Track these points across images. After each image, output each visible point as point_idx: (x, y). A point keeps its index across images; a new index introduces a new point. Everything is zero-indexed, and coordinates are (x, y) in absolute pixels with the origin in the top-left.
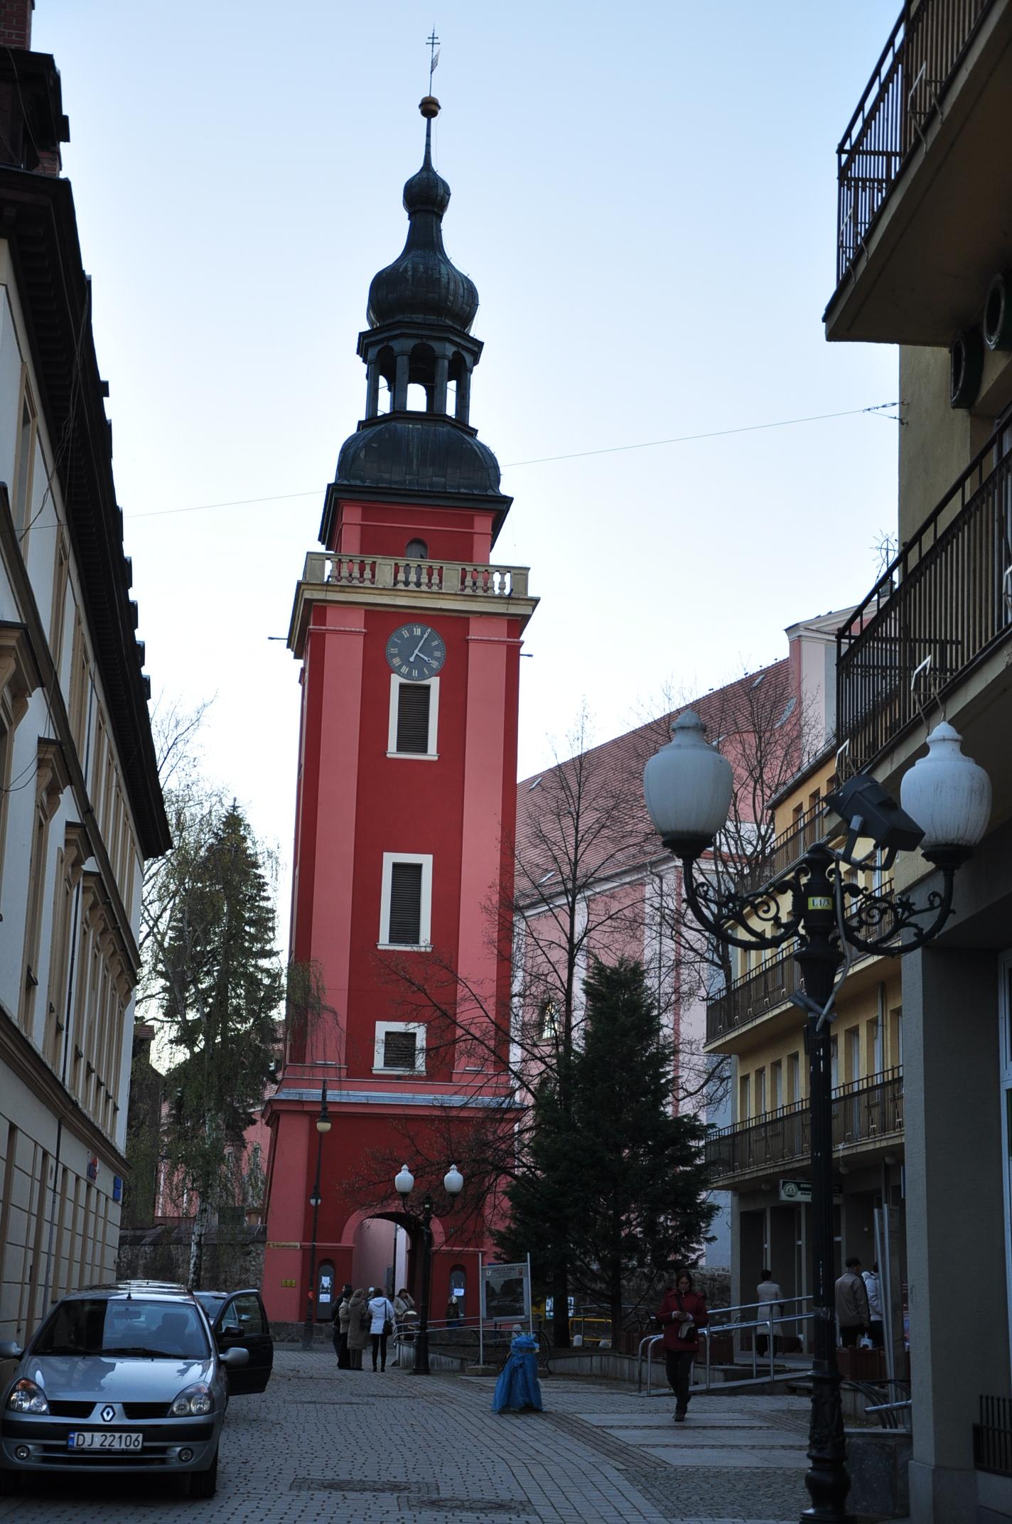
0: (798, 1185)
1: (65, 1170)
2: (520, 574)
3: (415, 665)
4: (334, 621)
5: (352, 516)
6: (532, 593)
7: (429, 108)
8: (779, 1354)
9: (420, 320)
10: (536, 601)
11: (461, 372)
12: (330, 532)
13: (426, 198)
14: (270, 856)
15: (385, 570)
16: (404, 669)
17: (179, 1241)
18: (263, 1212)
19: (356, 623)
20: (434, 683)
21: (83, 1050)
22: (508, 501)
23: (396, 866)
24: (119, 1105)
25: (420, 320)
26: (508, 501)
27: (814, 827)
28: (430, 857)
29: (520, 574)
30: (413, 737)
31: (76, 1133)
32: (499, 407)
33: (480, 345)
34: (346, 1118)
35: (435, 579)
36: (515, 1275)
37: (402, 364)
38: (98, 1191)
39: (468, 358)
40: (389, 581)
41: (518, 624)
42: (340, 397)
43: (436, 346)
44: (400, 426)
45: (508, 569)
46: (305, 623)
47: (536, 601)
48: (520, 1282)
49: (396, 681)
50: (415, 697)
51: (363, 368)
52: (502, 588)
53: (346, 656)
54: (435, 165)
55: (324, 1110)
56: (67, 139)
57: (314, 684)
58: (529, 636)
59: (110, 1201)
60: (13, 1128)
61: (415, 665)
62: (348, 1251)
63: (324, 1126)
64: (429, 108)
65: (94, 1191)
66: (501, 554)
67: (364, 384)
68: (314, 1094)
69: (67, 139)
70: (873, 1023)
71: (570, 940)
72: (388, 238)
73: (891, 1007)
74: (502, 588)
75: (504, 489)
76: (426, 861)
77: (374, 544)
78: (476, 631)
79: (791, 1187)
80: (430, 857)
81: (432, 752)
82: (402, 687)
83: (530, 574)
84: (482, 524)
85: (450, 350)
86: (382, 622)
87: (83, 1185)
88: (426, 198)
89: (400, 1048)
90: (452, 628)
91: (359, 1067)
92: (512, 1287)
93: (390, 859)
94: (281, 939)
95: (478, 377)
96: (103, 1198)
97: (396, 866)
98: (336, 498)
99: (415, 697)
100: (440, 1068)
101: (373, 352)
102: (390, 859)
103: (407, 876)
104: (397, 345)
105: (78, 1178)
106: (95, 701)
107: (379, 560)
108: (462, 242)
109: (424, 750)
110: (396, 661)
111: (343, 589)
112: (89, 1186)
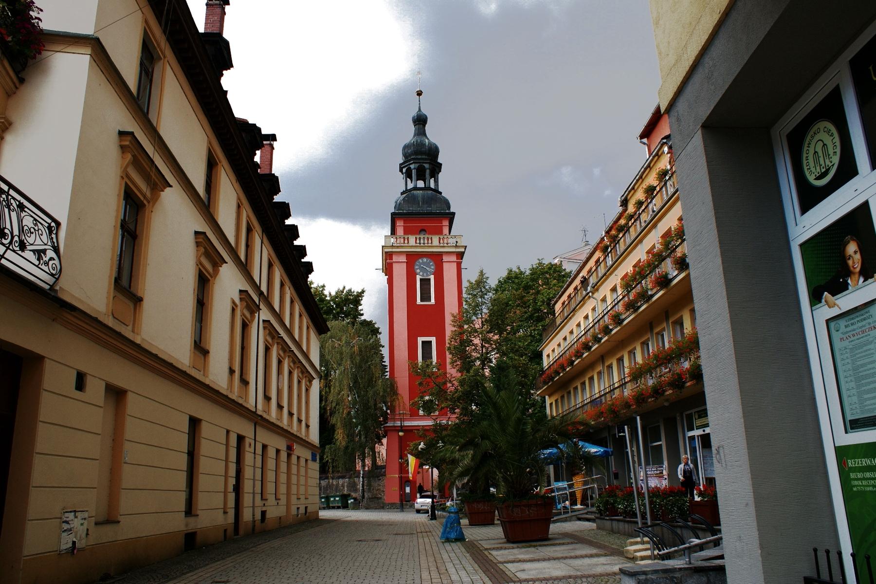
1: (265, 447)
3: (424, 270)
4: (395, 258)
5: (400, 223)
7: (419, 94)
8: (670, 277)
13: (420, 121)
14: (483, 438)
15: (412, 240)
20: (432, 277)
22: (454, 214)
23: (423, 342)
24: (311, 424)
26: (454, 214)
30: (425, 296)
31: (263, 426)
32: (448, 184)
37: (414, 172)
38: (298, 458)
39: (437, 170)
41: (461, 255)
44: (415, 192)
46: (386, 260)
49: (418, 278)
50: (425, 282)
53: (400, 271)
55: (402, 428)
56: (228, 4)
57: (390, 282)
59: (310, 462)
60: (228, 432)
61: (424, 270)
63: (401, 434)
64: (419, 94)
65: (294, 459)
67: (404, 182)
69: (228, 4)
70: (599, 373)
72: (408, 134)
73: (607, 364)
75: (452, 210)
76: (433, 339)
77: (408, 231)
78: (445, 258)
81: (433, 301)
82: (421, 280)
86: (412, 258)
87: (284, 455)
88: (420, 121)
90: (437, 258)
93: (420, 340)
97: (423, 342)
99: (425, 282)
101: (404, 170)
102: (420, 340)
103: (427, 345)
104: (412, 166)
105: (278, 451)
107: (410, 237)
108: (433, 134)
109: (430, 300)
110: (418, 271)
111: (398, 247)
112: (289, 456)
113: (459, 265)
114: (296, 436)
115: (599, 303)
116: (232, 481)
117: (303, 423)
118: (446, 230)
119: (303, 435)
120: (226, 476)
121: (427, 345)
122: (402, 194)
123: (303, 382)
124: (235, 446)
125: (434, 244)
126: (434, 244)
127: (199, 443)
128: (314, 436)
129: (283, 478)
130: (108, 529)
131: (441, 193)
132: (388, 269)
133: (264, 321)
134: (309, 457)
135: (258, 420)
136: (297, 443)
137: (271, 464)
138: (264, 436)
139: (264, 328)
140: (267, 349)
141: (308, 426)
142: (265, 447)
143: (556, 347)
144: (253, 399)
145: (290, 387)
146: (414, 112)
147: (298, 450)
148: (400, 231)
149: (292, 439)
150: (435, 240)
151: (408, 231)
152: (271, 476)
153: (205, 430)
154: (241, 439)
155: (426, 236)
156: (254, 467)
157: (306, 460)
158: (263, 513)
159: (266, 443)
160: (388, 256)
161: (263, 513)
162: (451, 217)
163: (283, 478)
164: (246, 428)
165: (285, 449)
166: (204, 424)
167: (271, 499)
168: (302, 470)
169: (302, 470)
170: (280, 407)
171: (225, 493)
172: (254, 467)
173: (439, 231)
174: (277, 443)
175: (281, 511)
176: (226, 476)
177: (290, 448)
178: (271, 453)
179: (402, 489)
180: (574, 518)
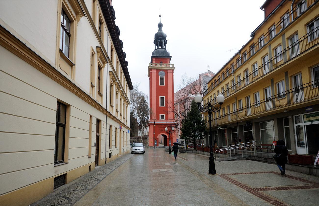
0: (220, 127)
2: (173, 64)
3: (162, 75)
4: (152, 71)
6: (174, 67)
7: (160, 16)
9: (160, 40)
10: (175, 67)
11: (165, 44)
12: (152, 61)
13: (160, 26)
15: (158, 65)
16: (161, 76)
17: (140, 138)
18: (149, 136)
19: (155, 71)
20: (164, 77)
21: (122, 114)
23: (161, 98)
24: (127, 120)
25: (160, 40)
27: (222, 78)
28: (160, 115)
29: (173, 64)
32: (170, 48)
33: (167, 41)
34: (157, 125)
35: (164, 66)
36: (183, 141)
38: (124, 131)
39: (166, 42)
40: (158, 66)
41: (173, 70)
42: (152, 47)
43: (162, 41)
45: (172, 64)
47: (175, 67)
48: (184, 141)
49: (160, 77)
50: (162, 79)
51: (154, 45)
52: (171, 66)
53: (154, 75)
54: (161, 22)
58: (174, 71)
59: (127, 133)
60: (91, 116)
62: (158, 139)
63: (155, 125)
64: (160, 16)
65: (122, 132)
66: (171, 63)
68: (153, 122)
71: (185, 99)
74: (171, 66)
76: (164, 97)
78: (168, 71)
79: (220, 127)
80: (160, 115)
81: (164, 85)
82: (160, 78)
83: (174, 64)
84: (169, 60)
85: (164, 41)
86: (158, 70)
87: (118, 130)
88: (160, 26)
89: (162, 117)
90: (166, 71)
91: (158, 119)
92: (182, 142)
93: (160, 97)
94: (149, 106)
95: (167, 45)
96: (125, 133)
97: (161, 98)
98: (152, 57)
99: (162, 79)
100: (167, 119)
102: (160, 97)
103: (162, 98)
105: (116, 129)
106: (120, 67)
107: (157, 64)
112: (120, 130)
113: (173, 73)
114: (123, 124)
115: (236, 77)
116: (94, 141)
117: (125, 119)
118: (168, 62)
119: (125, 123)
120: (90, 139)
121: (162, 98)
122: (154, 50)
123: (125, 104)
124: (96, 124)
125: (165, 66)
126: (165, 66)
127: (69, 119)
128: (129, 125)
129: (118, 139)
130: (207, 98)
131: (167, 50)
132: (150, 75)
133: (110, 71)
134: (127, 132)
135: (108, 114)
136: (123, 126)
137: (113, 133)
138: (110, 122)
139: (110, 75)
140: (111, 86)
141: (126, 121)
142: (111, 126)
143: (209, 97)
144: (104, 103)
145: (121, 105)
146: (159, 22)
147: (124, 129)
148: (154, 62)
149: (122, 124)
150: (165, 65)
151: (156, 62)
152: (113, 138)
153: (72, 112)
154: (98, 121)
155: (163, 64)
156: (106, 134)
157: (126, 133)
158: (110, 154)
159: (111, 125)
160: (150, 70)
161: (110, 154)
162: (170, 58)
163: (118, 139)
164: (102, 117)
165: (119, 128)
166: (71, 108)
167: (113, 147)
168: (125, 136)
169: (125, 136)
170: (117, 111)
171: (90, 147)
172: (106, 134)
173: (166, 62)
174: (115, 125)
175: (117, 152)
176: (90, 139)
177: (121, 128)
178: (113, 129)
179: (154, 142)
180: (245, 158)
